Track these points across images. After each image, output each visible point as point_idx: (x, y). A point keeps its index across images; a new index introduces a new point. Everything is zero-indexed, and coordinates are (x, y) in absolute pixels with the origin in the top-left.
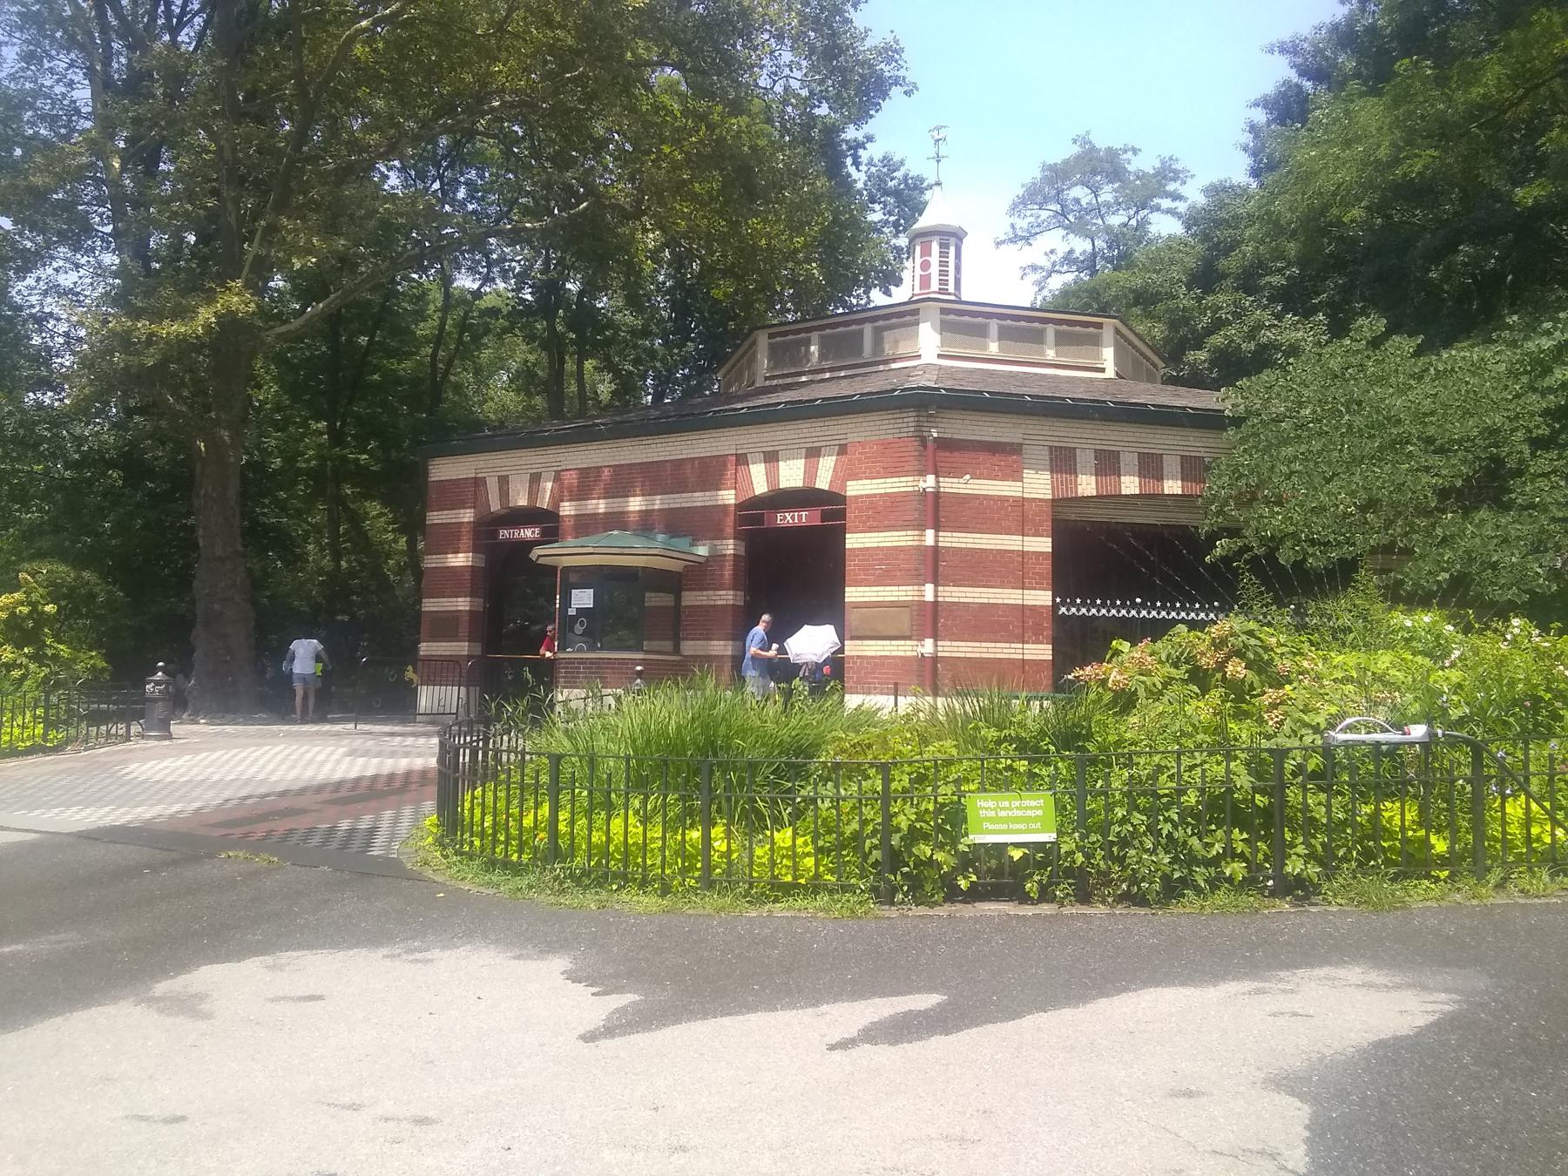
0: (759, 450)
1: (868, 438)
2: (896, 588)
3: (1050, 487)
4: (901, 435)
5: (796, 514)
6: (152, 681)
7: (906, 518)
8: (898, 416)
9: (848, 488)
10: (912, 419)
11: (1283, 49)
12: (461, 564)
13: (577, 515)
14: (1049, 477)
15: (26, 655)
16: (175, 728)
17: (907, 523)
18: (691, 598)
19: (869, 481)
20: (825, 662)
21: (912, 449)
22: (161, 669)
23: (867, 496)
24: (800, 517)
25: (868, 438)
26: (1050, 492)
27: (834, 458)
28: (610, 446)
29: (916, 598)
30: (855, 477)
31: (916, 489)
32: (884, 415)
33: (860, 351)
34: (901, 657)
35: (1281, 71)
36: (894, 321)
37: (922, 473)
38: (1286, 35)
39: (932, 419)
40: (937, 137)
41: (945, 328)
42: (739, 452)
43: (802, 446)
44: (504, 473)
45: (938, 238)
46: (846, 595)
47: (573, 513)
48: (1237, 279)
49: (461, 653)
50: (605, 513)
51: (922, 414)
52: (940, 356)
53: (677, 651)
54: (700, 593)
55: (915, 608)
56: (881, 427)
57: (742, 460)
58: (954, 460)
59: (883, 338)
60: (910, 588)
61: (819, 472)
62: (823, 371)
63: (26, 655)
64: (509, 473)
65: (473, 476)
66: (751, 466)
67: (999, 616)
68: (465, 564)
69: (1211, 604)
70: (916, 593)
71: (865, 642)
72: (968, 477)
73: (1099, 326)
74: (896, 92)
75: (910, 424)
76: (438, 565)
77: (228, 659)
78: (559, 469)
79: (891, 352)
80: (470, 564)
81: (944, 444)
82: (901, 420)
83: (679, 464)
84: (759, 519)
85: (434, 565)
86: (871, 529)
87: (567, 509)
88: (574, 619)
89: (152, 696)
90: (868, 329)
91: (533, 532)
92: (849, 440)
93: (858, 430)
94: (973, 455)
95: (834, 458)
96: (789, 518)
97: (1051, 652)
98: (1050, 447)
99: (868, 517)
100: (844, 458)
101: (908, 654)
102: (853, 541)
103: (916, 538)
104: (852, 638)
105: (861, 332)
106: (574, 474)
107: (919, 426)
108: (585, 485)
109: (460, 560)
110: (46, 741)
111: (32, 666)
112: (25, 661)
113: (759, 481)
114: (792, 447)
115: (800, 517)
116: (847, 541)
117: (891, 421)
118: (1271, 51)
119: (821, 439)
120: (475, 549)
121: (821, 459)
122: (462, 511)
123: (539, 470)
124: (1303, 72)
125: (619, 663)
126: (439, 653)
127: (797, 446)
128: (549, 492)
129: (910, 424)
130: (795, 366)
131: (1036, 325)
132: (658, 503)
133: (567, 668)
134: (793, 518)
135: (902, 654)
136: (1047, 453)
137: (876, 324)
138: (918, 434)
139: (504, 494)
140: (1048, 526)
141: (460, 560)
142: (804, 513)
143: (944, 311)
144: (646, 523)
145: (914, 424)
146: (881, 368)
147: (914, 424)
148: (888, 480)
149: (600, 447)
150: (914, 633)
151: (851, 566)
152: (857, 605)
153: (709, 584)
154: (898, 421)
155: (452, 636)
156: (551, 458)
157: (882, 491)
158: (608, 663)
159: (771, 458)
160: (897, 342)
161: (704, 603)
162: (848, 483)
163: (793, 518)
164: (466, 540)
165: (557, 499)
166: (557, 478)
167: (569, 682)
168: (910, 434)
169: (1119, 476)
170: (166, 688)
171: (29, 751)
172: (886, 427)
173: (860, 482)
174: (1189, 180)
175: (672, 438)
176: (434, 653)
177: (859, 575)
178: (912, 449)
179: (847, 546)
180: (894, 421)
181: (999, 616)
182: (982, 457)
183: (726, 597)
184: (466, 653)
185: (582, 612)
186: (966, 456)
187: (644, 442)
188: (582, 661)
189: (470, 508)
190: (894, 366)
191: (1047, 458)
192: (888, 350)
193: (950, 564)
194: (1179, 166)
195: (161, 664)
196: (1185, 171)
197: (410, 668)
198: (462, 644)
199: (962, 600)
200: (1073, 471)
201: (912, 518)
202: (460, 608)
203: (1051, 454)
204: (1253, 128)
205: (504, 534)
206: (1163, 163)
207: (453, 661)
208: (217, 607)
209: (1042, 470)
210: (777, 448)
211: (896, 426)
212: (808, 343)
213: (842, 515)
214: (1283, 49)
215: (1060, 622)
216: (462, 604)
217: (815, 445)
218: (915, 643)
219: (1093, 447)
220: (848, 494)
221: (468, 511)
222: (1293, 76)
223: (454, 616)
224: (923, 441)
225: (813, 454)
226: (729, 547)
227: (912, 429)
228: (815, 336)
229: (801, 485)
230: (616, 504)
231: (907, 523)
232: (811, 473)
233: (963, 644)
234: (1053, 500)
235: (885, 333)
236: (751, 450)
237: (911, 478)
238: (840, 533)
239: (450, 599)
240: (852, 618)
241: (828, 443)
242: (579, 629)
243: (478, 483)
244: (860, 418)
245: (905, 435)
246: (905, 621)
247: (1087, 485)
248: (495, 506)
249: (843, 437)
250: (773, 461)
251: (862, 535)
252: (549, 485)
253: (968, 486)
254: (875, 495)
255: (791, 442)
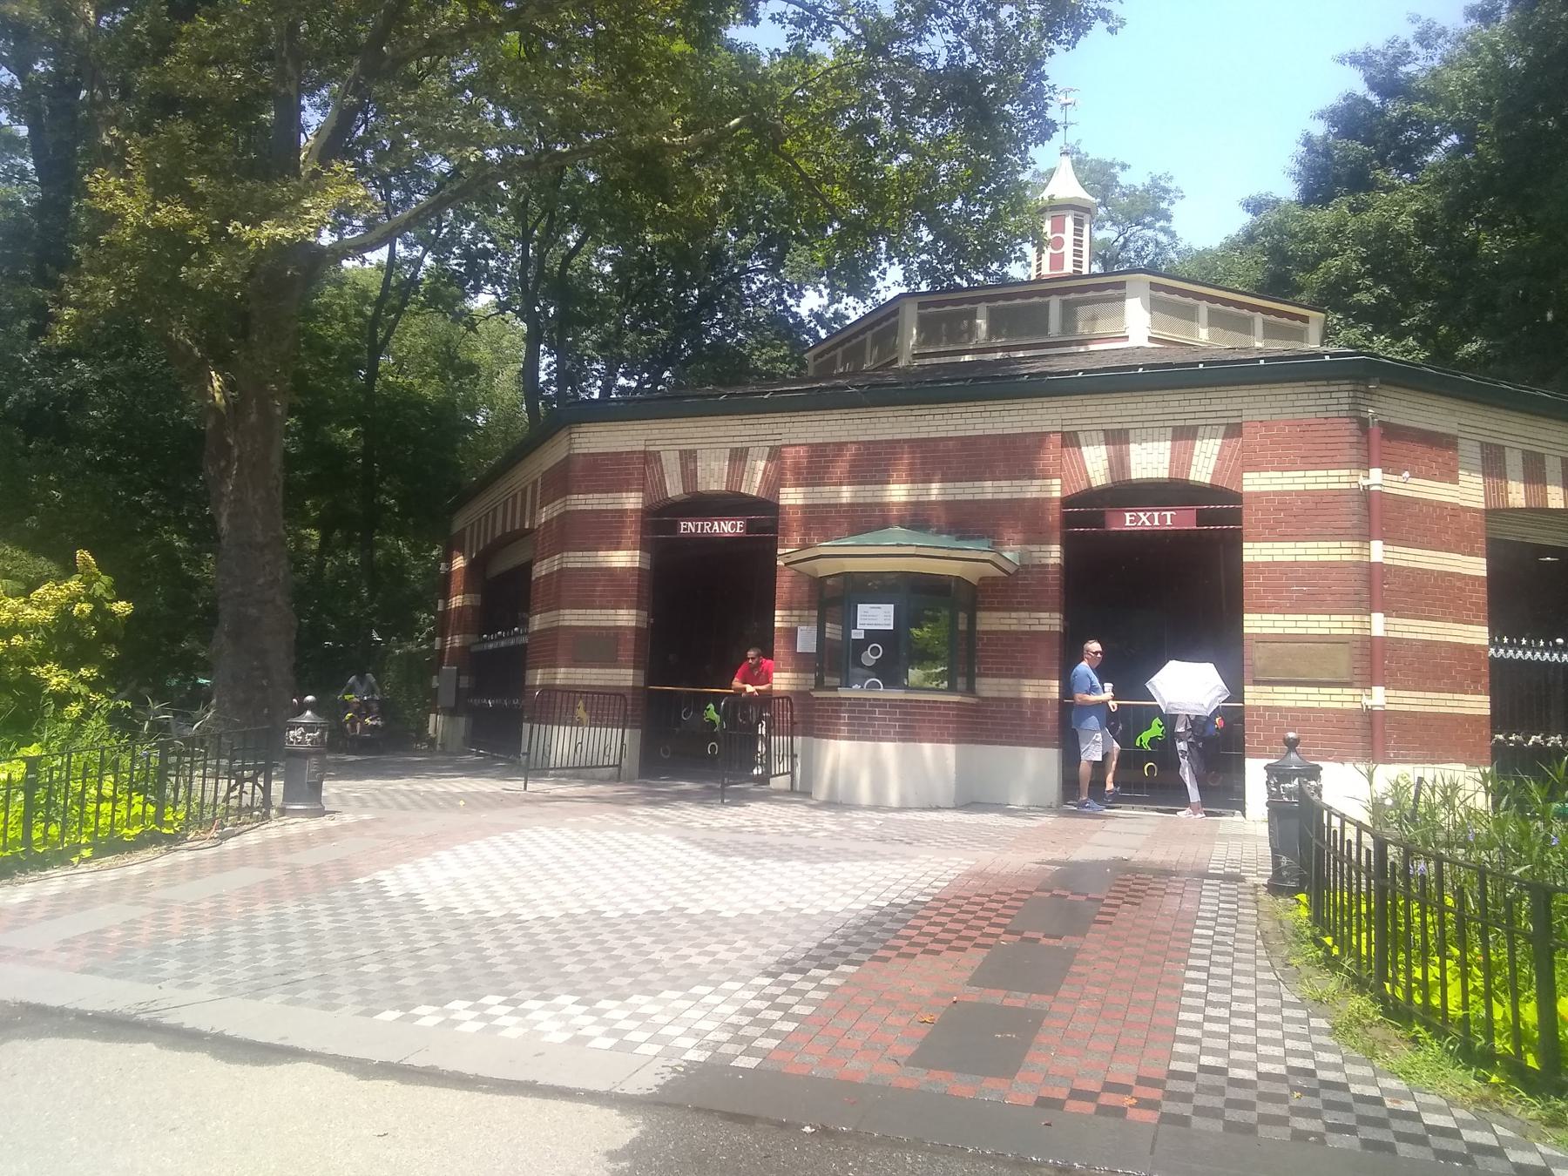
0: (1099, 427)
1: (1274, 417)
2: (1327, 617)
3: (1482, 493)
4: (1328, 414)
5: (1156, 514)
6: (301, 725)
7: (1339, 524)
8: (1324, 389)
9: (1245, 482)
10: (1346, 394)
11: (1354, 60)
12: (623, 565)
13: (807, 506)
14: (1481, 481)
15: (82, 680)
16: (331, 788)
17: (1338, 532)
18: (990, 621)
19: (1279, 474)
20: (1216, 712)
21: (1347, 433)
22: (310, 706)
23: (1275, 493)
24: (1162, 519)
25: (1274, 417)
26: (1483, 499)
27: (1219, 441)
28: (861, 416)
29: (1357, 632)
30: (1257, 467)
31: (1354, 486)
32: (1301, 387)
33: (1044, 330)
34: (1337, 710)
35: (1355, 83)
36: (1090, 294)
37: (1366, 465)
38: (1358, 45)
39: (1369, 396)
40: (1064, 101)
41: (1155, 306)
42: (1066, 429)
43: (1167, 424)
44: (689, 447)
45: (1073, 212)
46: (1245, 624)
47: (800, 502)
48: (1320, 292)
49: (622, 684)
50: (851, 505)
51: (1359, 388)
52: (1151, 339)
53: (970, 690)
54: (1005, 614)
55: (1355, 644)
56: (1296, 403)
57: (1070, 440)
58: (1391, 451)
59: (1075, 313)
60: (1349, 618)
61: (1195, 461)
62: (994, 350)
63: (82, 680)
64: (697, 447)
65: (642, 448)
66: (1084, 449)
67: (1443, 658)
68: (629, 565)
69: (1537, 642)
70: (1357, 625)
71: (1277, 689)
72: (1406, 474)
73: (1305, 319)
74: (1099, 26)
75: (1342, 401)
76: (585, 565)
77: (265, 683)
78: (777, 443)
79: (1086, 331)
80: (637, 565)
81: (1392, 432)
82: (1328, 395)
83: (968, 443)
84: (1098, 520)
85: (579, 565)
86: (1283, 538)
87: (792, 497)
88: (861, 646)
89: (302, 748)
90: (1055, 303)
91: (734, 526)
92: (1244, 418)
93: (1258, 405)
94: (1411, 446)
95: (1219, 441)
96: (1144, 518)
97: (1488, 705)
98: (1482, 443)
99: (1278, 522)
100: (1236, 443)
101: (1347, 706)
102: (1253, 552)
103: (1355, 551)
104: (1256, 683)
105: (1047, 305)
106: (802, 451)
107: (1355, 406)
108: (816, 466)
109: (623, 559)
110: (161, 824)
111: (94, 697)
112: (84, 690)
113: (1095, 464)
114: (1152, 424)
115: (1162, 519)
116: (1245, 552)
117: (1312, 396)
118: (1342, 61)
119: (1197, 415)
120: (643, 546)
121: (1198, 443)
122: (624, 495)
123: (744, 445)
124: (1373, 85)
125: (945, 708)
126: (587, 683)
127: (1161, 424)
128: (760, 475)
129: (1342, 401)
130: (955, 343)
131: (1245, 312)
132: (935, 491)
133: (854, 712)
134: (1151, 519)
135: (1338, 705)
136: (1478, 450)
137: (1066, 297)
138: (1353, 413)
139: (689, 475)
140: (1481, 544)
141: (623, 559)
142: (1168, 514)
143: (1154, 286)
144: (917, 518)
145: (1350, 400)
146: (1074, 349)
147: (1350, 400)
148: (1309, 473)
149: (844, 417)
150: (1356, 678)
151: (1251, 585)
152: (1264, 639)
153: (1019, 603)
154: (1323, 396)
155: (612, 662)
156: (765, 429)
157: (1301, 488)
158: (918, 707)
159: (1117, 438)
160: (1094, 318)
161: (1013, 628)
162: (1245, 475)
163: (1151, 519)
164: (631, 532)
165: (775, 482)
166: (775, 454)
167: (858, 732)
168: (1342, 414)
169: (1545, 485)
170: (321, 736)
171: (140, 843)
172: (1303, 403)
173: (1264, 474)
174: (1178, 201)
175: (960, 408)
176: (578, 682)
177: (1266, 598)
178: (1347, 433)
179: (1245, 559)
180: (1317, 396)
181: (1443, 658)
182: (1420, 449)
183: (1050, 621)
184: (630, 684)
185: (872, 635)
186: (1404, 447)
187: (915, 413)
188: (877, 703)
189: (637, 491)
190: (1092, 347)
191: (1479, 456)
192: (1082, 329)
193: (1393, 587)
194: (1172, 185)
195: (310, 698)
196: (1178, 190)
197: (711, 706)
198: (623, 671)
199: (1406, 636)
200: (1503, 476)
201: (1348, 524)
202: (619, 624)
203: (1482, 452)
204: (1308, 141)
205: (688, 527)
206: (1153, 179)
207: (614, 694)
208: (253, 611)
209: (1474, 471)
210: (1125, 426)
211: (1319, 402)
212: (972, 315)
213: (1236, 517)
214: (1354, 60)
215: (1495, 663)
216: (626, 617)
217: (1189, 423)
218: (1358, 691)
219: (1521, 446)
220: (1245, 489)
221: (633, 494)
222: (1361, 89)
223: (613, 635)
224: (1363, 424)
225: (1185, 435)
226: (1054, 554)
227: (1347, 407)
228: (982, 308)
229: (1166, 475)
230: (867, 494)
231: (1338, 532)
232: (1181, 460)
233: (1406, 693)
234: (1487, 511)
235: (1080, 309)
236: (1085, 428)
237: (1346, 472)
238: (1234, 543)
239: (603, 611)
240: (1255, 656)
241: (1210, 421)
242: (869, 658)
243: (650, 458)
244: (1264, 390)
245: (1335, 414)
246: (1343, 662)
247: (1517, 494)
248: (674, 488)
249: (1236, 413)
250: (1121, 443)
251: (1269, 545)
252: (761, 465)
253: (1408, 487)
254: (1289, 493)
255: (1151, 418)
